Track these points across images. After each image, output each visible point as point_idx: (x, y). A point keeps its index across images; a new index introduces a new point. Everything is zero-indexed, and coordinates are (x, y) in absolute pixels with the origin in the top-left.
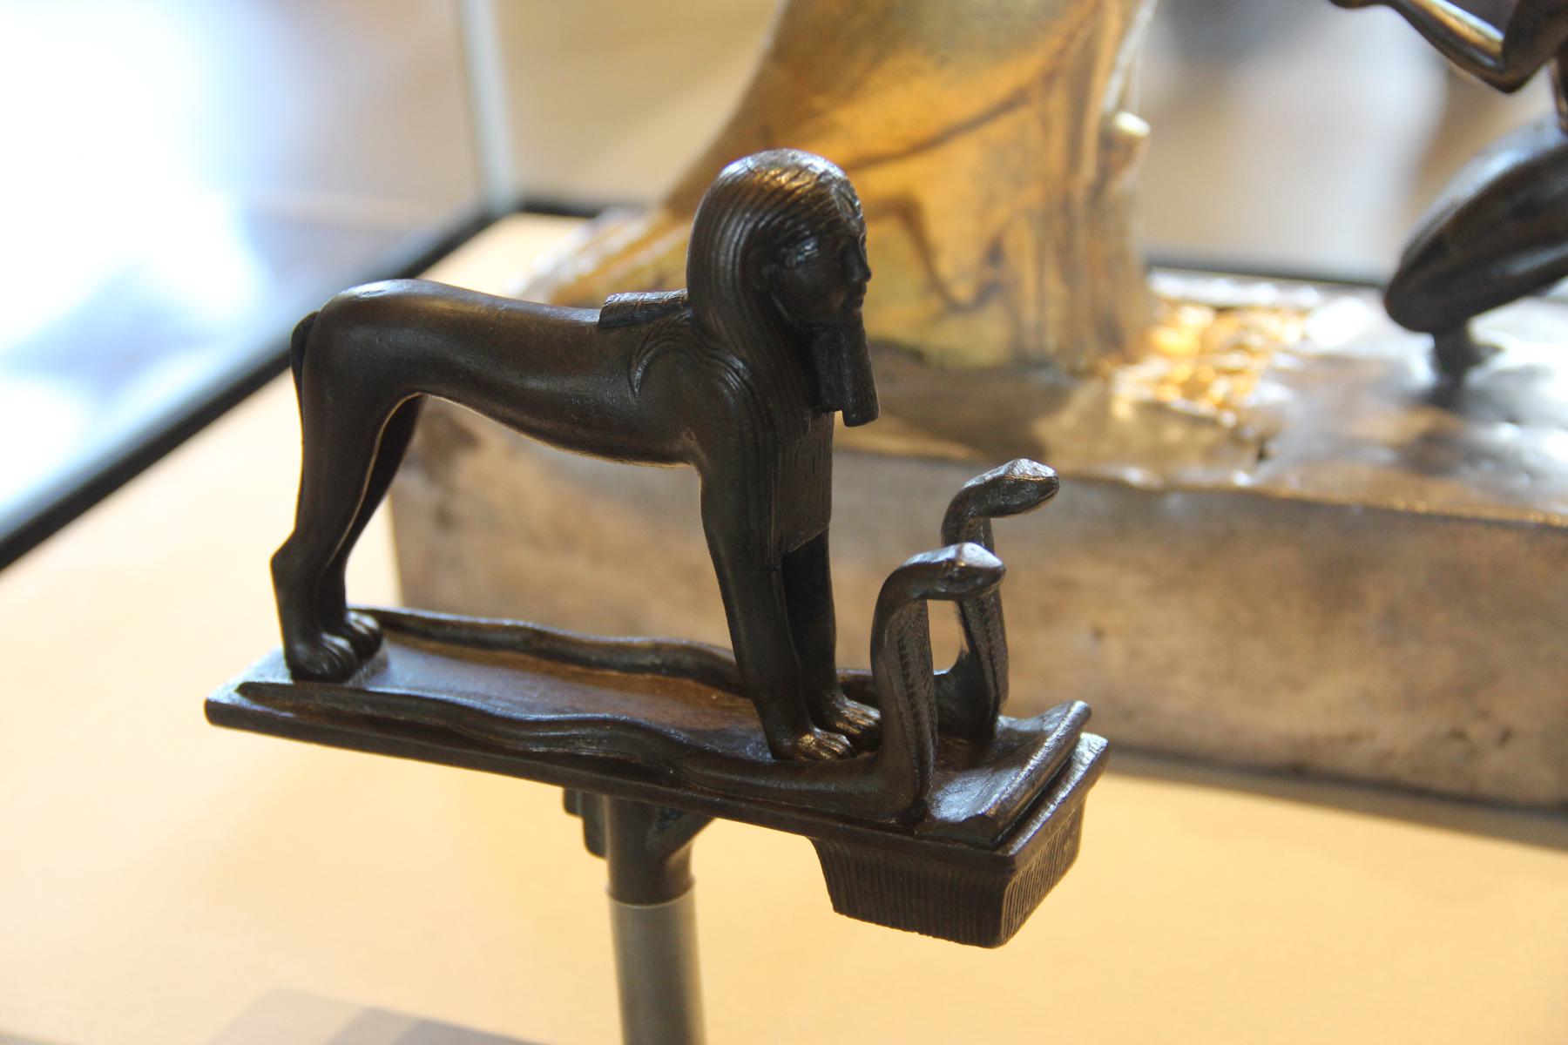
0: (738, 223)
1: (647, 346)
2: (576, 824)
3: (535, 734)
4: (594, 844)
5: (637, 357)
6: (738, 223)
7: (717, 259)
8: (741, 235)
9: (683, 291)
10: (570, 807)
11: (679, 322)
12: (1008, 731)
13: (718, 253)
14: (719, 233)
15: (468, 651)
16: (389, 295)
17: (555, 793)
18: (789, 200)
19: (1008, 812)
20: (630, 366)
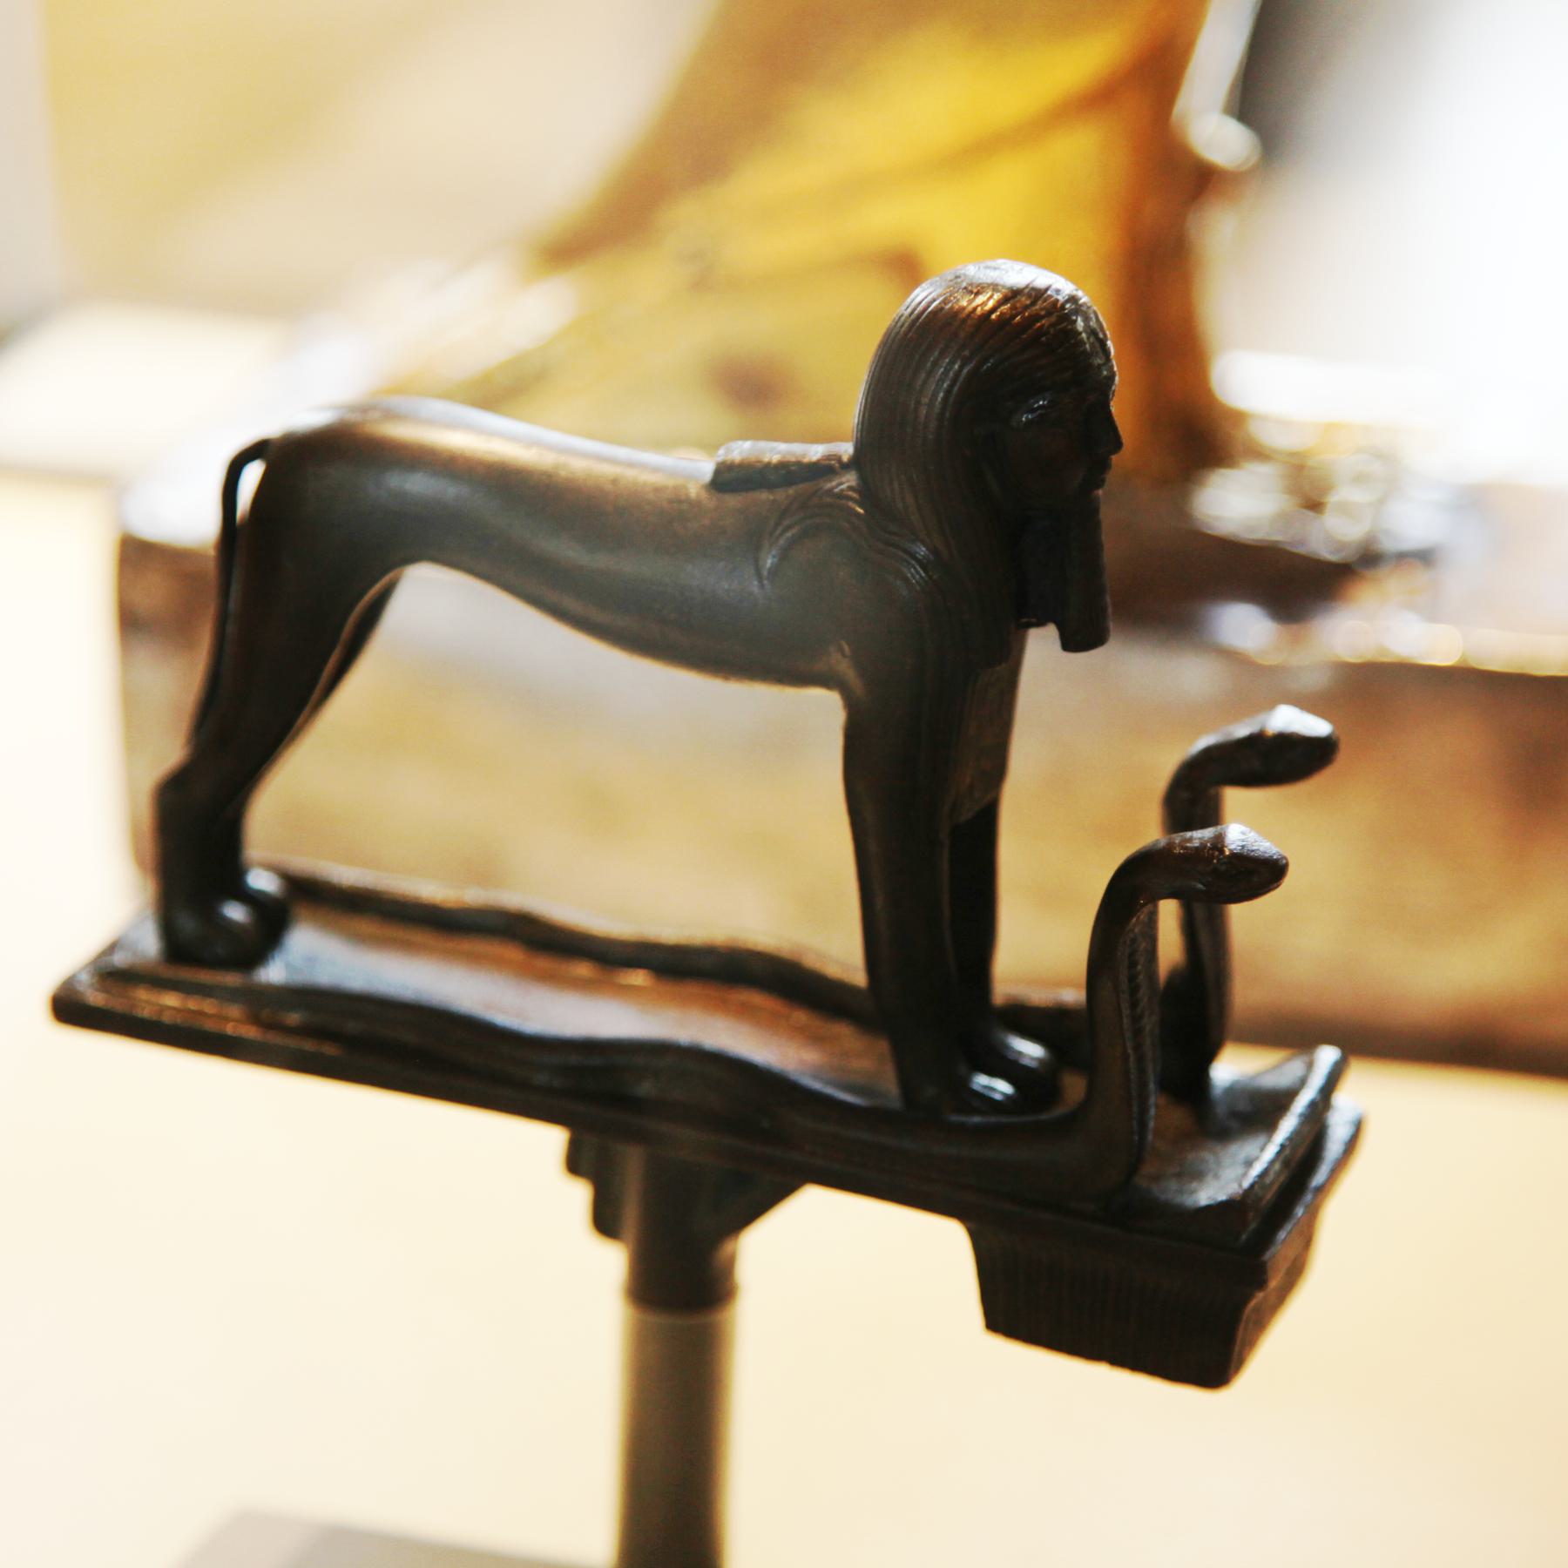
0: (952, 363)
1: (786, 522)
2: (579, 1194)
3: (193, 1004)
4: (605, 1221)
5: (771, 534)
6: (952, 363)
7: (916, 410)
8: (930, 374)
9: (846, 450)
10: (575, 1164)
11: (836, 490)
12: (1233, 1091)
13: (918, 403)
14: (923, 376)
15: (418, 936)
16: (1259, 544)
17: (551, 1140)
18: (918, 324)
19: (1261, 1199)
20: (758, 548)
